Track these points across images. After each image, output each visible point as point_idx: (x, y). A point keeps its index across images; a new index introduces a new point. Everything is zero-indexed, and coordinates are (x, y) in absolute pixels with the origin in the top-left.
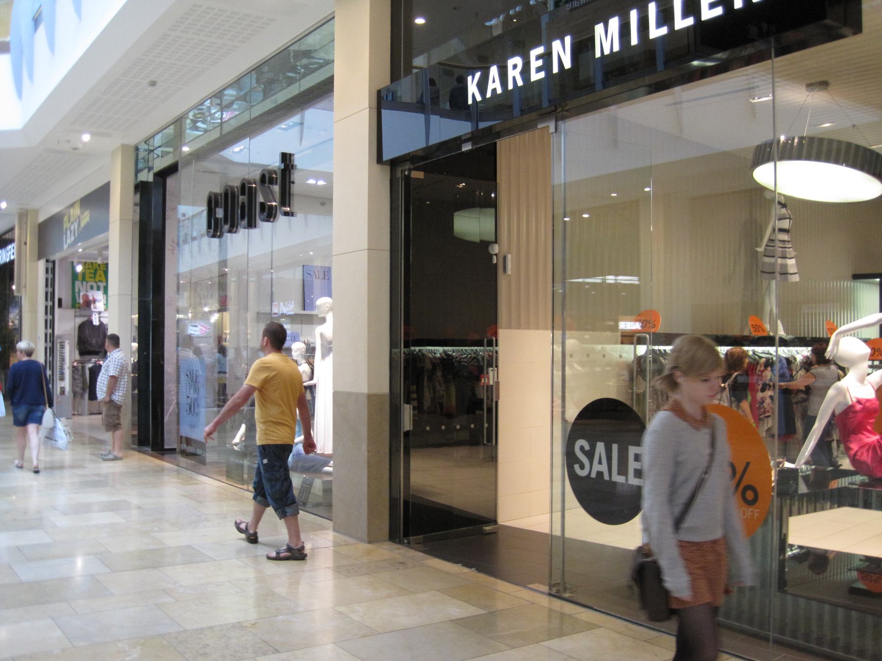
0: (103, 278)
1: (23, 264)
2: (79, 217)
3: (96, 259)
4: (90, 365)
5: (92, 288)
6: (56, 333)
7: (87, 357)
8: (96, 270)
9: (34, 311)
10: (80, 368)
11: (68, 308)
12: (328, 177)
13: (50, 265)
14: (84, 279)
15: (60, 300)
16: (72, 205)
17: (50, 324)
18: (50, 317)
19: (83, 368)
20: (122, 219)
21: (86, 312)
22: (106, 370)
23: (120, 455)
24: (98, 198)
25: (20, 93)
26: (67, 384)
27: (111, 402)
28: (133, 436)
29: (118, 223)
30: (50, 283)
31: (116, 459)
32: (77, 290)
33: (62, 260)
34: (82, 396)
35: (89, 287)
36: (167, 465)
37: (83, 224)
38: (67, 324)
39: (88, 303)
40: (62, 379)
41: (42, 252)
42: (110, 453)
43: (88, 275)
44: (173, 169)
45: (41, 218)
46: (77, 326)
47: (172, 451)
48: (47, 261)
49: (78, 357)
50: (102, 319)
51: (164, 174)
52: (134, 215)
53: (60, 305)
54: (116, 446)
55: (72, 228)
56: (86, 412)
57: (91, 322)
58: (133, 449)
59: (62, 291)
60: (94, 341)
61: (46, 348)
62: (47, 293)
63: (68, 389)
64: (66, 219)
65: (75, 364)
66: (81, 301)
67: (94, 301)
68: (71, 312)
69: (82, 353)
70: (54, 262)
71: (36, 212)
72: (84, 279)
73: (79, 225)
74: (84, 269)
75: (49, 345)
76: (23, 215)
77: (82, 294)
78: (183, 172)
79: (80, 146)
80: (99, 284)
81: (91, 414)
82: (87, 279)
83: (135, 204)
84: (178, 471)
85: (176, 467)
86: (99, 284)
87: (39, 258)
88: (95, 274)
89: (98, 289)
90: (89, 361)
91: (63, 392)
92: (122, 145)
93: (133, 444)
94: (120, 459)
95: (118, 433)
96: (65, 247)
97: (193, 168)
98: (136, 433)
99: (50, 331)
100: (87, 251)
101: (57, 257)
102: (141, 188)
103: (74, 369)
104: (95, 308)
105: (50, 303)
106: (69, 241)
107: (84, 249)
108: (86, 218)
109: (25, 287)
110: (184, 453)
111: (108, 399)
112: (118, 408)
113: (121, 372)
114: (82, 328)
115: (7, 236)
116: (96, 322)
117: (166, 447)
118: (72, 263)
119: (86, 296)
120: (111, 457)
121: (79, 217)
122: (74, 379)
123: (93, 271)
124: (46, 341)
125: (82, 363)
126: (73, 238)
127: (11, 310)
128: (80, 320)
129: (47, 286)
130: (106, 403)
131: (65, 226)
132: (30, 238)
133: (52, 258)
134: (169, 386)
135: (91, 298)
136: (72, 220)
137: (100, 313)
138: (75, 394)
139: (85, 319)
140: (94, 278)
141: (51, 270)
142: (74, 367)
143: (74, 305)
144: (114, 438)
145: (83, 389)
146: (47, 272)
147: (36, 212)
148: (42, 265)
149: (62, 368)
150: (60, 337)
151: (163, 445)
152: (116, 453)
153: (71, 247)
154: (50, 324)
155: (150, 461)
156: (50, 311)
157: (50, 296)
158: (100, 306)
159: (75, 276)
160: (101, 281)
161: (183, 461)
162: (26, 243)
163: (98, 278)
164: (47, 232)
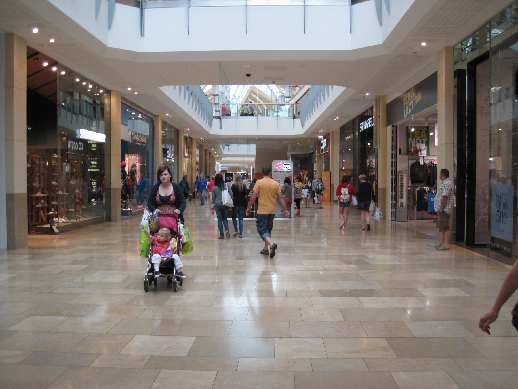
0: (425, 136)
1: (378, 130)
2: (414, 98)
3: (424, 124)
4: (418, 189)
5: (418, 142)
6: (398, 170)
7: (416, 185)
8: (421, 131)
9: (385, 157)
10: (412, 191)
11: (403, 155)
12: (122, 203)
13: (395, 129)
14: (413, 137)
15: (400, 150)
16: (409, 91)
17: (395, 164)
18: (394, 160)
19: (414, 191)
20: (447, 95)
21: (415, 157)
22: (440, 192)
23: (448, 247)
24: (429, 84)
25: (381, 23)
26: (404, 200)
27: (443, 212)
28: (453, 234)
29: (444, 98)
30: (394, 140)
31: (445, 249)
32: (409, 144)
33: (402, 125)
34: (413, 208)
35: (417, 141)
36: (476, 254)
37: (417, 101)
38: (404, 164)
39: (417, 151)
40: (402, 197)
41: (389, 121)
42: (441, 246)
43: (416, 134)
44: (485, 57)
45: (388, 101)
46: (410, 165)
47: (485, 246)
48: (393, 126)
49: (410, 184)
50: (425, 161)
51: (473, 64)
52: (453, 91)
53: (400, 153)
54: (446, 242)
55: (410, 104)
56: (415, 218)
57: (419, 163)
58: (453, 243)
59: (401, 144)
60: (420, 175)
61: (392, 179)
62: (392, 146)
63: (405, 204)
64: (405, 99)
65: (409, 188)
66: (413, 150)
67: (420, 150)
68: (406, 157)
69: (412, 182)
70: (396, 127)
71: (385, 97)
72: (413, 137)
73: (414, 102)
74: (416, 130)
75: (394, 177)
76: (378, 100)
77: (413, 146)
78: (492, 59)
79: (419, 50)
80: (423, 139)
81: (417, 219)
82: (416, 137)
83: (455, 86)
84: (488, 260)
85: (487, 258)
86: (423, 139)
87: (388, 125)
88: (420, 133)
89: (422, 142)
90: (417, 187)
91: (402, 205)
92: (446, 47)
93: (453, 240)
94: (448, 250)
95: (447, 233)
96: (405, 117)
97: (500, 55)
98: (454, 232)
99: (394, 169)
100: (418, 119)
101: (398, 123)
102: (459, 74)
103: (409, 192)
104: (421, 154)
105: (394, 152)
106: (407, 113)
107: (415, 118)
108: (419, 97)
109: (380, 142)
110: (494, 249)
111: (441, 211)
112: (448, 216)
113: (450, 193)
114: (413, 166)
115: (367, 114)
116: (422, 163)
117: (476, 243)
118: (407, 127)
119: (415, 147)
120: (442, 248)
121: (414, 98)
122: (408, 198)
123: (419, 132)
124: (392, 175)
125: (414, 188)
126: (410, 111)
127: (368, 157)
128: (411, 162)
129: (392, 141)
130: (440, 213)
131: (404, 104)
132: (382, 114)
133: (395, 124)
134: (479, 203)
135: (418, 148)
136: (409, 99)
137: (423, 157)
138: (409, 207)
139: (415, 161)
140: (420, 136)
141: (395, 132)
142: (408, 190)
143: (408, 152)
144: (444, 236)
145: (414, 204)
146: (392, 133)
147: (385, 97)
148: (389, 128)
149: (402, 191)
150: (401, 172)
151: (474, 242)
152: (445, 245)
153: (408, 116)
154: (395, 164)
155: (465, 252)
156: (394, 156)
157: (394, 147)
158: (424, 153)
159: (408, 134)
160: (424, 138)
161: (493, 253)
162: (379, 117)
163: (422, 136)
164: (393, 109)
